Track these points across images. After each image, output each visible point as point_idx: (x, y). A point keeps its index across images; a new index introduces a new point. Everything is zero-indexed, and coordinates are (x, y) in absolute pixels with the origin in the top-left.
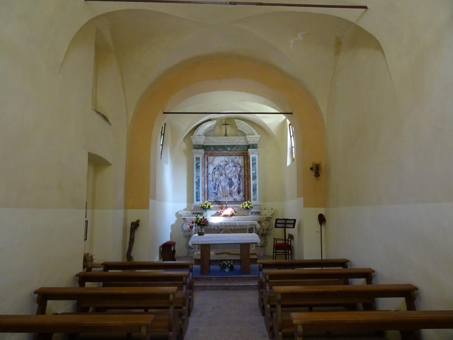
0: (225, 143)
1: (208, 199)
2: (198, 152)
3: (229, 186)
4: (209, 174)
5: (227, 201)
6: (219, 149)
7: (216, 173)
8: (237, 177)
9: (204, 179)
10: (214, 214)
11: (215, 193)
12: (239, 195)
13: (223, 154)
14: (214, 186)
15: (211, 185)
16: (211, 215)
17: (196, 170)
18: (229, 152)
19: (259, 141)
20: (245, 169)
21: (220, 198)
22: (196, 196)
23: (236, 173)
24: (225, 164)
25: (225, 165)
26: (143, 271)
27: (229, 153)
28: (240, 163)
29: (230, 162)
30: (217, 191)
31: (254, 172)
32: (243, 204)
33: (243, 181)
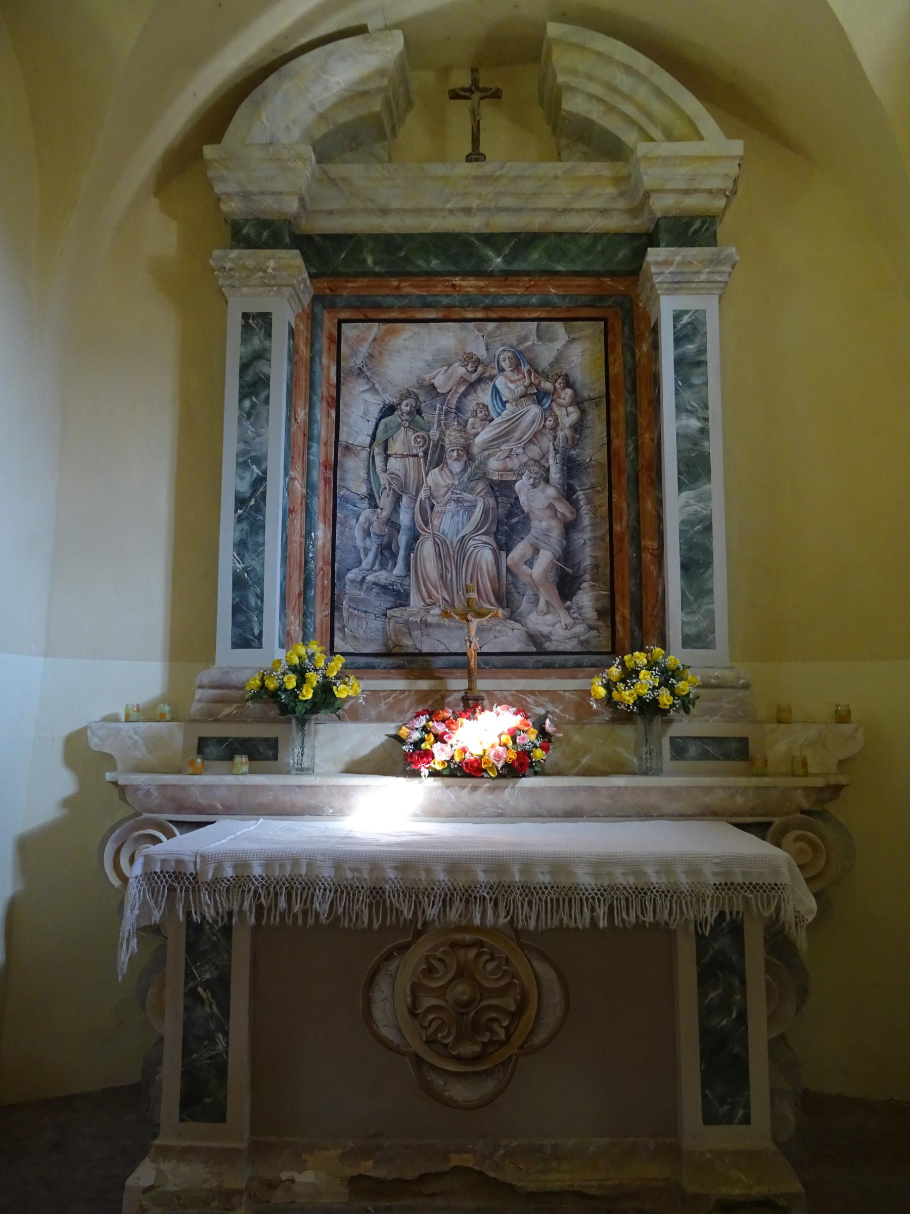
0: (468, 211)
1: (337, 634)
2: (260, 270)
3: (491, 540)
4: (347, 448)
5: (479, 654)
6: (421, 263)
7: (396, 447)
8: (555, 475)
9: (309, 486)
10: (365, 751)
11: (384, 587)
12: (568, 609)
13: (448, 307)
14: (380, 536)
15: (358, 534)
16: (345, 759)
17: (241, 407)
18: (492, 290)
19: (729, 185)
20: (613, 415)
21: (427, 625)
22: (237, 609)
23: (546, 442)
24: (463, 380)
25: (462, 389)
26: (559, 681)
27: (497, 296)
28: (578, 376)
29: (505, 365)
30: (403, 573)
31: (694, 424)
32: (615, 672)
33: (597, 503)
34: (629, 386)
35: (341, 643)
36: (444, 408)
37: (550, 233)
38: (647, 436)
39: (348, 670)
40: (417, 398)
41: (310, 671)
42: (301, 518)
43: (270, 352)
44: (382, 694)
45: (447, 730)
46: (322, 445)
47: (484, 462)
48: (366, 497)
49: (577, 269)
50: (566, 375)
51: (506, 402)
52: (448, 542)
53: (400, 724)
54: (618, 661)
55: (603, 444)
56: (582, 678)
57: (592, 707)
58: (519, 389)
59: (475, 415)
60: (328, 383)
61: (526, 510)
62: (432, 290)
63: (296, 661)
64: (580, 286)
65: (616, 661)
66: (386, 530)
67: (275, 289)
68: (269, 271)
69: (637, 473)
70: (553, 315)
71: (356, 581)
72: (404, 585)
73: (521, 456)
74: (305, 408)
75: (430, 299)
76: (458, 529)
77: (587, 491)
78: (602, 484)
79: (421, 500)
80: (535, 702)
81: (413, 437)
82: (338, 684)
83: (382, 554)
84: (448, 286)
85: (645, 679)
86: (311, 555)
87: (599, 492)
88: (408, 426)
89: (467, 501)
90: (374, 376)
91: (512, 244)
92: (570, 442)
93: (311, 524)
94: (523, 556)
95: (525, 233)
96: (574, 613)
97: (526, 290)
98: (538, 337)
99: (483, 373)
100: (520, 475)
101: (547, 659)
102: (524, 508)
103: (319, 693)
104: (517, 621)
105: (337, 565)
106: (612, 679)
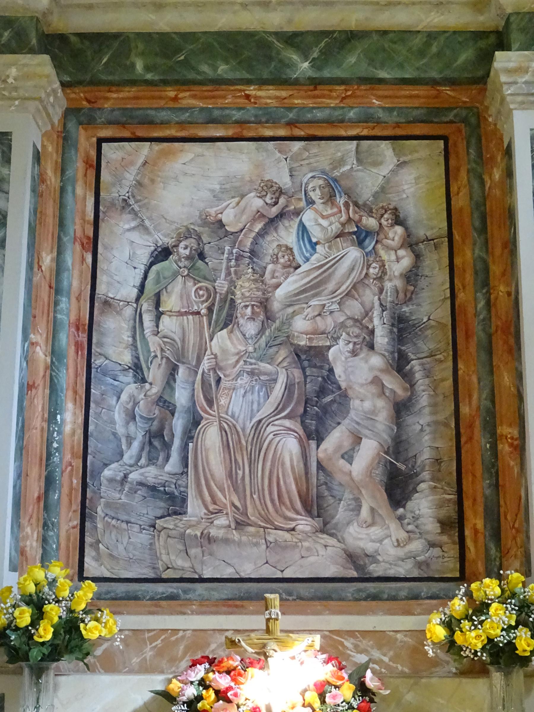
4: (106, 303)
6: (205, 68)
11: (153, 489)
12: (401, 518)
13: (240, 123)
15: (118, 416)
20: (457, 261)
21: (210, 540)
24: (259, 215)
25: (258, 227)
26: (389, 618)
27: (303, 108)
29: (315, 195)
33: (438, 376)
34: (477, 224)
35: (94, 564)
36: (235, 251)
37: (371, 32)
38: (502, 288)
39: (102, 602)
40: (199, 238)
41: (50, 603)
42: (44, 397)
43: (9, 182)
44: (147, 635)
45: (232, 684)
46: (74, 300)
47: (288, 321)
48: (130, 368)
49: (407, 76)
50: (396, 209)
51: (316, 243)
52: (239, 430)
53: (171, 676)
54: (463, 590)
55: (445, 299)
56: (419, 614)
57: (427, 653)
58: (333, 227)
59: (275, 261)
60: (83, 219)
61: (343, 385)
62: (220, 101)
63: (31, 588)
64: (411, 97)
65: (460, 591)
66: (157, 412)
67: (17, 103)
68: (10, 80)
69: (490, 336)
70: (377, 132)
71: (116, 480)
72: (180, 486)
73: (336, 314)
74: (52, 252)
75: (216, 113)
76: (252, 410)
77: (424, 360)
78: (445, 351)
79: (203, 372)
80: (356, 646)
81: (194, 289)
82: (86, 621)
83: (150, 443)
84: (240, 97)
85: (497, 615)
86: (55, 445)
87: (441, 361)
88: (188, 275)
89: (265, 374)
90: (144, 210)
91: (323, 44)
92: (401, 295)
93: (57, 404)
94: (339, 447)
95: (340, 32)
96: (409, 524)
97: (341, 101)
98: (358, 160)
99: (287, 206)
100: (336, 339)
101: (371, 587)
102: (340, 383)
103: (62, 632)
104: (332, 535)
105: (89, 458)
106: (454, 614)
